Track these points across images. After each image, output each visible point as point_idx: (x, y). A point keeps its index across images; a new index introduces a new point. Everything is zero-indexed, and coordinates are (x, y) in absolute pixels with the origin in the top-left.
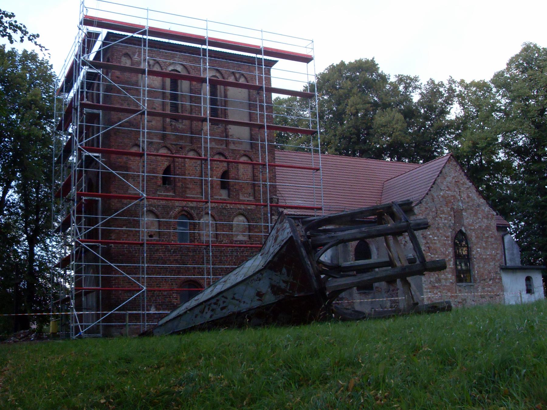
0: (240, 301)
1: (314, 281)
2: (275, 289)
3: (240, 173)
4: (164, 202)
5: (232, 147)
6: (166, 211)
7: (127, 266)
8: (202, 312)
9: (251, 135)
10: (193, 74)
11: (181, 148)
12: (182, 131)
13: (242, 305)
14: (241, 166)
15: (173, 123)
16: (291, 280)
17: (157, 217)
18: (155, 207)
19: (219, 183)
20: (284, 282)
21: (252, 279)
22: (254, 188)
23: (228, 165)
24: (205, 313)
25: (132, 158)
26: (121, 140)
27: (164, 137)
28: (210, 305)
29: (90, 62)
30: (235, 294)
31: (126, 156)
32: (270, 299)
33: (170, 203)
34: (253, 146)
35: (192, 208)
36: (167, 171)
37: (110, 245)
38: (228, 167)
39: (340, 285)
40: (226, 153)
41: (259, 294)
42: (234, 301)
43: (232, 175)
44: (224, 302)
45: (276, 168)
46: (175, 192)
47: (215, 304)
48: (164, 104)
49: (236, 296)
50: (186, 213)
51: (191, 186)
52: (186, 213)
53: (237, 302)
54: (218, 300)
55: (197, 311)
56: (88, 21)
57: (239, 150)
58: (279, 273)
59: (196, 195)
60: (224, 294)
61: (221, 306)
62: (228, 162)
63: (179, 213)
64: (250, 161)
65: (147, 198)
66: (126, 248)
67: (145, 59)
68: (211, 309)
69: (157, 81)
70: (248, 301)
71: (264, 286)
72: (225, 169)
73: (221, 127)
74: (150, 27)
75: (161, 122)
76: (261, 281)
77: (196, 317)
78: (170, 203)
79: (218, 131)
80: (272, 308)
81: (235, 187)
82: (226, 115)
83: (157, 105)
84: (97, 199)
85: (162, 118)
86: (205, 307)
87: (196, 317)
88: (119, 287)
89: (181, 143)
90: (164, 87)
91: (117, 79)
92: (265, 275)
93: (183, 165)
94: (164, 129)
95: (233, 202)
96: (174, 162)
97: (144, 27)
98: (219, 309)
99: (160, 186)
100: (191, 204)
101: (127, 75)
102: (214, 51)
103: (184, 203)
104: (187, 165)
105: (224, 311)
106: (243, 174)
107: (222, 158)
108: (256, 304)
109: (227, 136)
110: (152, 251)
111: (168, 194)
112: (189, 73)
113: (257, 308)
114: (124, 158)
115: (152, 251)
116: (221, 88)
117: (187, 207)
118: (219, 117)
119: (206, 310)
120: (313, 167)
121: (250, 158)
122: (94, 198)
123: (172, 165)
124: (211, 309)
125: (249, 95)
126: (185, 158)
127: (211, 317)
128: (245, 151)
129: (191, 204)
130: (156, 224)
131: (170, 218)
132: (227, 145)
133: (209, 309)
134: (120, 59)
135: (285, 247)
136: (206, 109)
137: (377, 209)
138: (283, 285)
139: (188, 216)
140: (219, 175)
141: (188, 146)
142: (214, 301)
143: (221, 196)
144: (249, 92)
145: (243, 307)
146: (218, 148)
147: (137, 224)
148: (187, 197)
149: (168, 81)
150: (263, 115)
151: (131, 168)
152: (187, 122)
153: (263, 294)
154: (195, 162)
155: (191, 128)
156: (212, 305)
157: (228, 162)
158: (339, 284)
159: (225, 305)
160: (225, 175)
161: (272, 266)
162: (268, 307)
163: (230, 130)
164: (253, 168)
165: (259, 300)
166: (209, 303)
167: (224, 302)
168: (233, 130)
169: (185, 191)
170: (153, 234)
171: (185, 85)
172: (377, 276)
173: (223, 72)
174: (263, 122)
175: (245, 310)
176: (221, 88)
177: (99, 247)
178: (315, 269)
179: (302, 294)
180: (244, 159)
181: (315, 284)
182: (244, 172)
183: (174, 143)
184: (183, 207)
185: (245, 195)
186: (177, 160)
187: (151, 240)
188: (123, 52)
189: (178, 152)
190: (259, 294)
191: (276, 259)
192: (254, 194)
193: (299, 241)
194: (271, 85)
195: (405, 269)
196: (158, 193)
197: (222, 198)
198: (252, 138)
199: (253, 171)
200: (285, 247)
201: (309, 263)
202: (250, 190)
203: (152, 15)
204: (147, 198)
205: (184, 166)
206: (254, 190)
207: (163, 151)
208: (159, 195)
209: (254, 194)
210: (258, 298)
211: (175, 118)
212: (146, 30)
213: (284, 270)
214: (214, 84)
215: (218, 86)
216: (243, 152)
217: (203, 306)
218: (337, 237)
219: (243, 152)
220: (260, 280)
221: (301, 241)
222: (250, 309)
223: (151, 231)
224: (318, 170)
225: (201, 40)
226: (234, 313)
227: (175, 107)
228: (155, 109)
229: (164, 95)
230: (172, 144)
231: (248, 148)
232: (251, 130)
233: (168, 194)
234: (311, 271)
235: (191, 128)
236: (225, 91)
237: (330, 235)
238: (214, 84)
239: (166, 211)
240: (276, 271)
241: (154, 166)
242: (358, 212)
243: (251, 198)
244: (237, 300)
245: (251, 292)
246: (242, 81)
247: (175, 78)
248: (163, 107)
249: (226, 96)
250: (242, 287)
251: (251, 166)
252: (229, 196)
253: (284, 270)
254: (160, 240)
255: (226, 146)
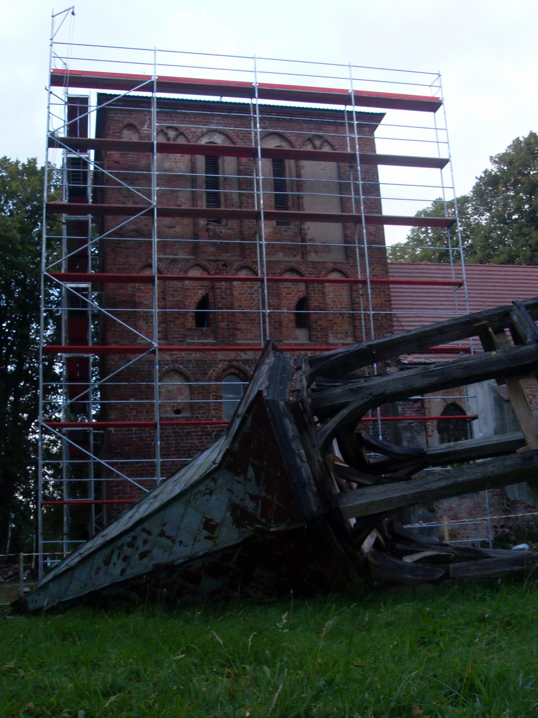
0: (173, 541)
1: (310, 495)
2: (240, 515)
3: (329, 301)
4: (198, 355)
5: (313, 257)
6: (202, 369)
7: (137, 463)
8: (107, 562)
9: (345, 236)
10: (240, 144)
11: (225, 265)
12: (228, 237)
13: (178, 549)
14: (329, 288)
15: (211, 227)
16: (263, 494)
17: (187, 379)
18: (182, 364)
19: (293, 317)
20: (253, 498)
21: (196, 491)
22: (354, 323)
23: (307, 288)
24: (111, 565)
25: (143, 288)
26: (122, 260)
27: (195, 249)
28: (121, 548)
29: (62, 139)
30: (164, 525)
31: (132, 285)
32: (229, 536)
33: (208, 357)
34: (349, 253)
35: (246, 362)
36: (204, 303)
37: (109, 429)
38: (307, 291)
39: (372, 504)
40: (303, 269)
41: (210, 526)
42: (164, 541)
43: (314, 303)
44: (145, 542)
45: (391, 286)
46: (216, 338)
47: (130, 545)
48: (194, 197)
49: (167, 529)
50: (236, 372)
51: (243, 327)
52: (236, 372)
53: (168, 542)
54: (135, 538)
55: (99, 560)
56: (58, 79)
57: (325, 263)
58: (241, 479)
59: (253, 340)
60: (146, 525)
61: (139, 551)
62: (307, 282)
63: (224, 371)
64: (344, 279)
65: (160, 350)
66: (135, 434)
67: (153, 129)
68: (122, 556)
69: (179, 164)
70: (188, 544)
71: (217, 507)
72: (301, 295)
73: (293, 227)
74: (160, 77)
75: (191, 226)
76: (214, 497)
77: (97, 573)
78: (208, 357)
79: (288, 233)
80: (236, 556)
81: (319, 323)
82: (300, 206)
83: (183, 200)
84: (85, 355)
85: (191, 220)
86: (112, 552)
87: (97, 573)
88: (124, 498)
89: (226, 257)
90: (193, 170)
91: (115, 164)
92: (220, 481)
93: (229, 292)
94: (196, 236)
95: (318, 347)
96: (213, 288)
97: (150, 77)
98: (137, 557)
99: (190, 329)
100: (243, 356)
101: (132, 156)
102: (274, 106)
103: (232, 355)
104: (235, 293)
105: (145, 561)
106: (334, 302)
107: (296, 277)
108: (203, 546)
109: (303, 240)
110: (180, 436)
111: (205, 341)
112: (234, 144)
113: (204, 555)
114: (130, 287)
115: (180, 436)
116: (290, 164)
117: (238, 361)
118: (287, 210)
119: (115, 558)
120: (454, 280)
121: (344, 274)
122: (81, 355)
123: (210, 295)
124: (122, 556)
125: (339, 172)
126: (231, 280)
127: (123, 571)
128: (335, 263)
129: (243, 356)
130: (187, 392)
131: (210, 380)
132: (304, 255)
133: (119, 555)
134: (120, 133)
135: (249, 420)
136: (262, 199)
137: (476, 320)
138: (250, 505)
139: (241, 375)
140: (291, 306)
141: (236, 261)
142: (127, 539)
143: (297, 339)
144: (339, 167)
145: (180, 553)
146: (287, 262)
147: (149, 392)
148: (236, 344)
149: (200, 160)
150: (359, 199)
151: (141, 303)
152: (234, 223)
153: (217, 525)
154: (249, 287)
155: (241, 232)
156: (125, 548)
157: (307, 282)
158: (369, 500)
159: (147, 547)
160: (302, 303)
161: (230, 463)
162: (227, 553)
163: (308, 232)
164: (351, 290)
165: (208, 538)
166: (119, 543)
167: (145, 542)
168: (312, 229)
169: (234, 335)
170: (181, 407)
171: (229, 166)
172: (460, 479)
173: (293, 139)
174: (360, 212)
175: (182, 561)
176: (290, 164)
177: (90, 432)
178: (317, 466)
179: (283, 527)
180: (335, 276)
181: (313, 504)
182: (335, 297)
183: (213, 258)
184: (230, 361)
185: (339, 336)
186: (218, 284)
187: (178, 418)
188: (125, 123)
189: (220, 271)
190: (210, 526)
191: (237, 446)
192: (355, 332)
193: (282, 403)
194: (375, 151)
195: (531, 458)
196: (188, 341)
197: (297, 342)
198: (347, 239)
199: (351, 295)
200: (249, 420)
201: (302, 451)
202: (347, 327)
203: (161, 58)
204: (160, 350)
205: (232, 294)
206: (354, 327)
207: (195, 273)
208: (189, 344)
209: (355, 332)
210: (205, 533)
211: (217, 218)
212: (153, 82)
213: (251, 472)
214: (277, 158)
215: (287, 161)
216: (331, 265)
217: (107, 551)
218: (368, 388)
219: (331, 265)
220: (210, 493)
221: (287, 403)
222: (192, 559)
223: (179, 404)
224: (460, 284)
225: (245, 90)
226: (170, 568)
227: (214, 199)
228: (180, 206)
229: (194, 181)
230: (209, 261)
231: (339, 257)
232: (345, 228)
233: (205, 341)
234: (306, 471)
235: (241, 232)
236: (298, 170)
237: (354, 386)
238: (277, 158)
239: (202, 369)
240: (238, 475)
241: (180, 298)
242: (433, 330)
243: (349, 340)
244: (169, 538)
245: (193, 520)
246: (327, 149)
247: (213, 155)
248: (193, 202)
249: (299, 175)
250: (177, 510)
251: (346, 287)
252: (310, 339)
253: (251, 472)
254: (192, 417)
255: (303, 258)
